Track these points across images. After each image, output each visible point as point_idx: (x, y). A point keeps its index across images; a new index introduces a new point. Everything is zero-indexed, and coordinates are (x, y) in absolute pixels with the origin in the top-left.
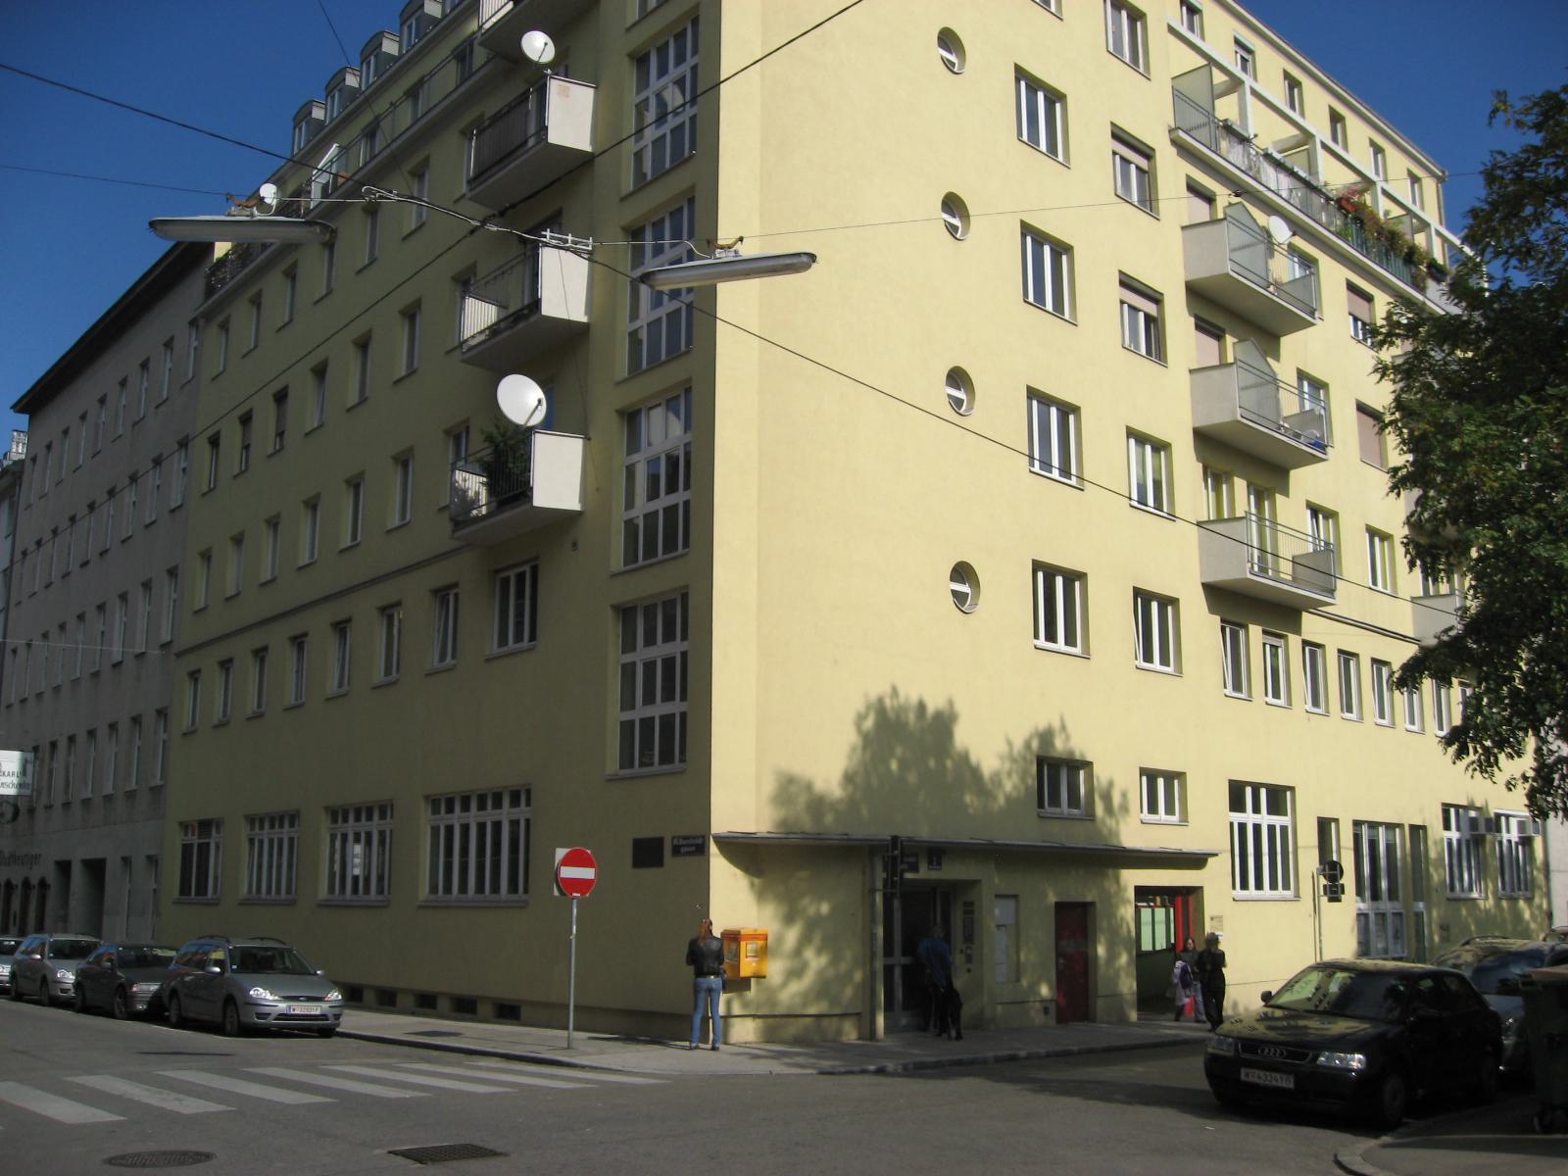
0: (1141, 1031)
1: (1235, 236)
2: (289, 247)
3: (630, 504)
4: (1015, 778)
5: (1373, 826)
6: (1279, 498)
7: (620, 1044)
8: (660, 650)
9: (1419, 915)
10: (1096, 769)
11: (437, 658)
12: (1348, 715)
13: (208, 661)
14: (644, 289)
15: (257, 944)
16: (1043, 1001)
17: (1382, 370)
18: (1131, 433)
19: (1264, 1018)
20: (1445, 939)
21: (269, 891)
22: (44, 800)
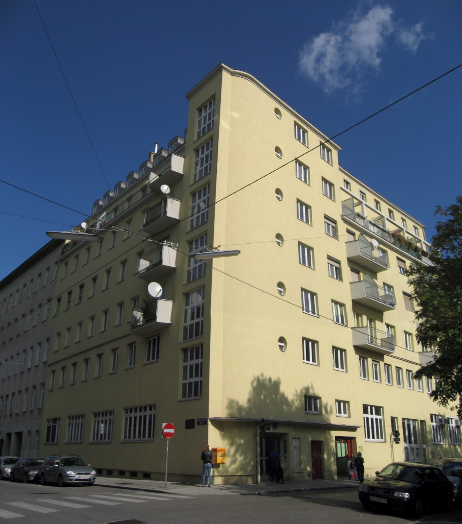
0: (339, 483)
1: (361, 245)
2: (86, 243)
3: (185, 321)
4: (298, 401)
5: (409, 420)
6: (377, 322)
7: (180, 485)
8: (195, 362)
9: (424, 449)
10: (323, 399)
11: (128, 365)
12: (399, 386)
13: (58, 368)
14: (192, 259)
15: (70, 457)
16: (308, 472)
17: (411, 283)
18: (333, 301)
19: (377, 480)
20: (433, 457)
21: (74, 440)
22: (3, 414)
